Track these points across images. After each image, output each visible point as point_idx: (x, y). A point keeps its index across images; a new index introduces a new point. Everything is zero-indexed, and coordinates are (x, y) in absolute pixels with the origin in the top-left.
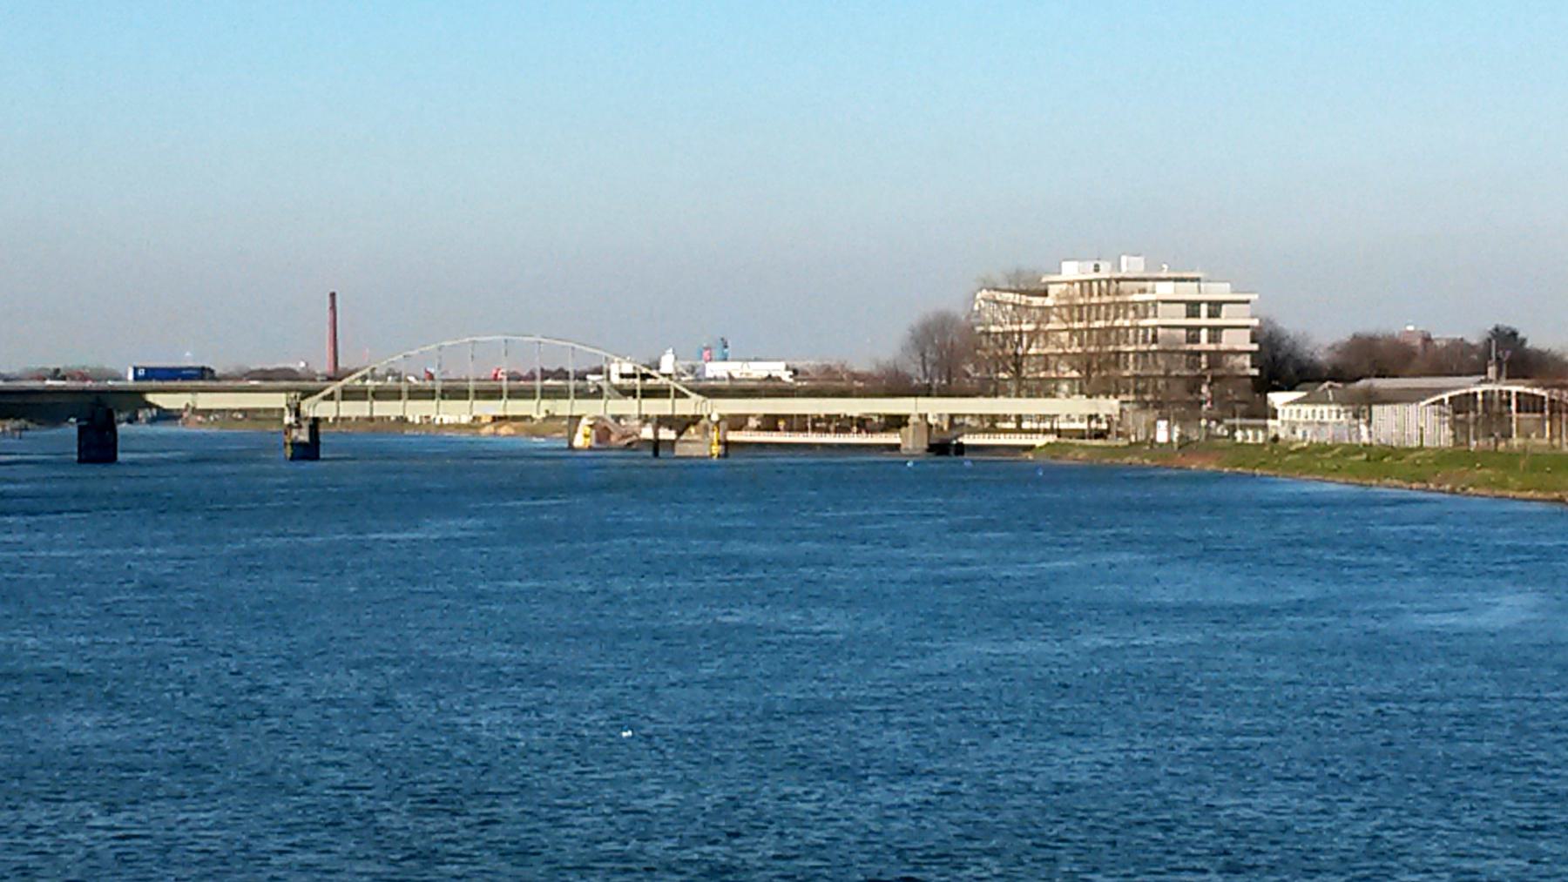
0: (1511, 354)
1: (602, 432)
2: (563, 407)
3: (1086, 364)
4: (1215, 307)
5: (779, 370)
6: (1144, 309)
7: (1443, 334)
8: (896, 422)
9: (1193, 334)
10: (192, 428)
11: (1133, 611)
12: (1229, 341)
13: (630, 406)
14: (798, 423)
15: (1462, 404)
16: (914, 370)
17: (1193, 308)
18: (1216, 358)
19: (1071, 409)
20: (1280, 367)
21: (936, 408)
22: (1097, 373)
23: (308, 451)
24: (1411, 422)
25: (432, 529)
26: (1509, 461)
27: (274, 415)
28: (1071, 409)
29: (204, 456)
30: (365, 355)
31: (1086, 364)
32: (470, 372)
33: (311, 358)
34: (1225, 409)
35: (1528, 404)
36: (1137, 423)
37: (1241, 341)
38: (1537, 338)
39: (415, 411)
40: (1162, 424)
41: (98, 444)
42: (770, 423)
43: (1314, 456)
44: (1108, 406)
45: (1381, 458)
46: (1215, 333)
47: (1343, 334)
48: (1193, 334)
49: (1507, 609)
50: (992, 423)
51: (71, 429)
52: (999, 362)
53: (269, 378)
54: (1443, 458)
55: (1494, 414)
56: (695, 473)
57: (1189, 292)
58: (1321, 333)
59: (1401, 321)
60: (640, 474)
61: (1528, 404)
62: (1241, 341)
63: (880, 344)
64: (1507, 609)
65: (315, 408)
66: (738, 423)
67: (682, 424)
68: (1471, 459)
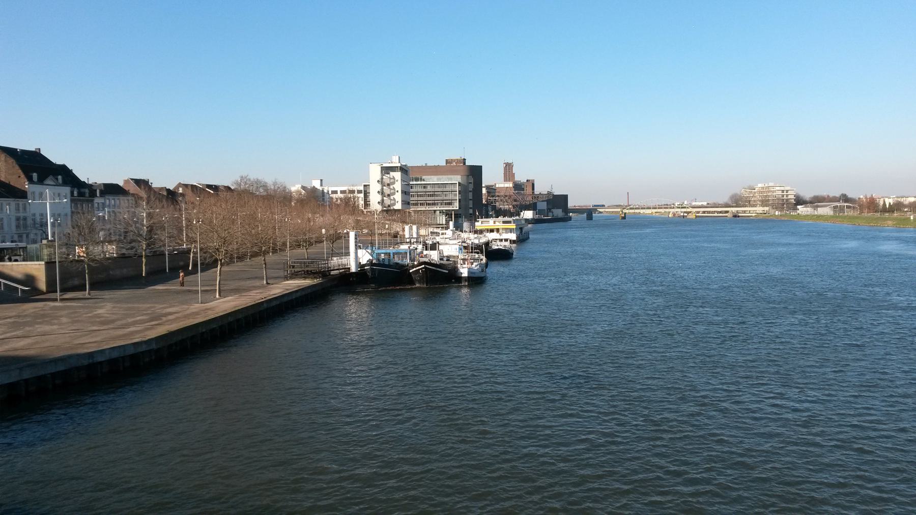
0: (845, 198)
1: (674, 215)
2: (667, 210)
3: (762, 201)
4: (787, 191)
5: (705, 204)
6: (773, 192)
7: (831, 195)
8: (727, 212)
9: (783, 196)
10: (605, 214)
11: (779, 244)
12: (790, 197)
13: (679, 210)
14: (709, 212)
15: (835, 207)
16: (730, 203)
17: (783, 191)
18: (787, 200)
19: (759, 209)
20: (799, 201)
21: (734, 210)
22: (764, 203)
23: (624, 218)
24: (825, 211)
25: (648, 231)
26: (845, 217)
27: (618, 212)
28: (759, 209)
29: (608, 219)
30: (634, 202)
31: (762, 201)
32: (652, 205)
33: (624, 202)
34: (789, 209)
35: (848, 207)
36: (772, 212)
37: (792, 197)
38: (850, 195)
39: (642, 211)
40: (407, 228)
41: (590, 217)
42: (704, 212)
43: (806, 217)
44: (766, 209)
45: (819, 217)
46: (787, 196)
47: (812, 195)
48: (783, 196)
49: (852, 244)
50: (745, 212)
51: (585, 215)
52: (746, 201)
53: (618, 206)
54: (831, 217)
55: (842, 209)
56: (691, 222)
57: (782, 188)
58: (807, 195)
59: (824, 193)
60: (681, 221)
61: (848, 207)
62: (792, 197)
63: (725, 199)
64: (852, 244)
65: (625, 211)
66: (698, 212)
67: (688, 213)
68: (837, 217)
